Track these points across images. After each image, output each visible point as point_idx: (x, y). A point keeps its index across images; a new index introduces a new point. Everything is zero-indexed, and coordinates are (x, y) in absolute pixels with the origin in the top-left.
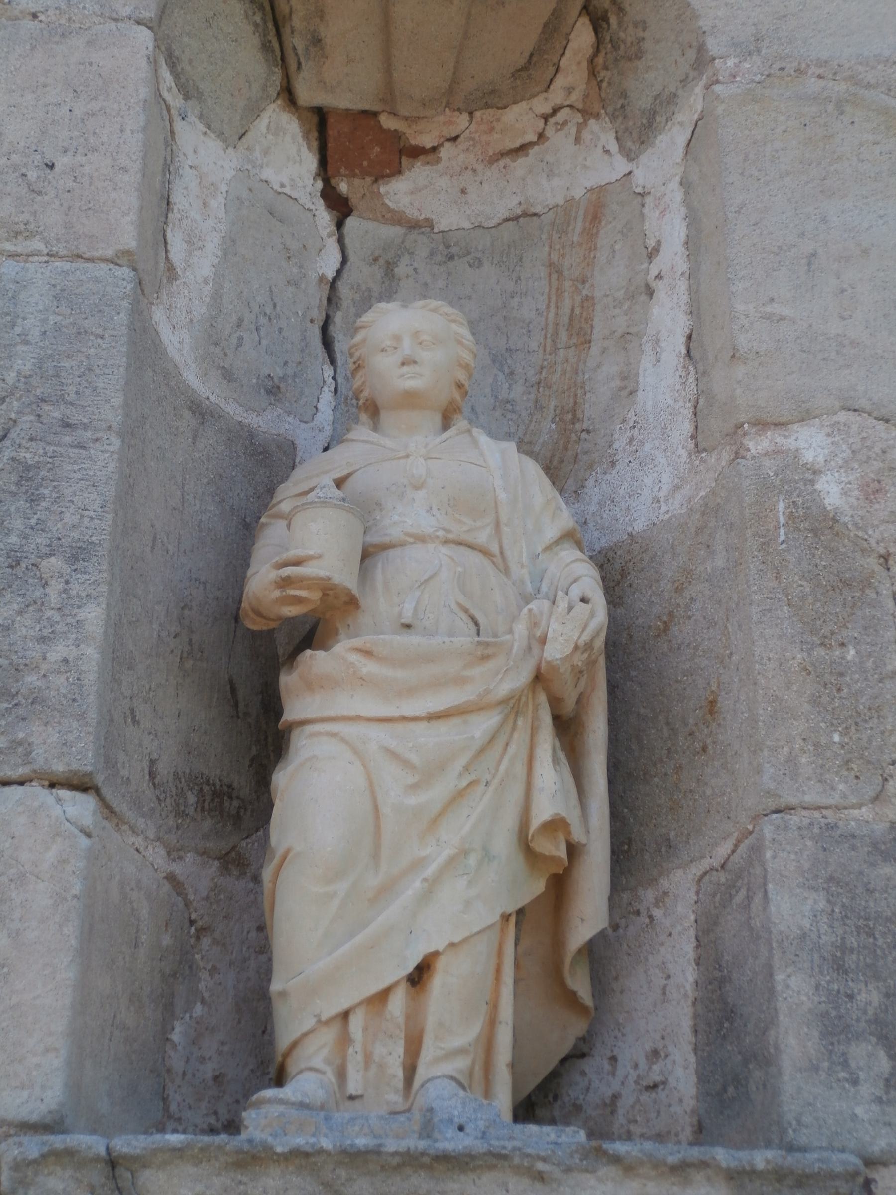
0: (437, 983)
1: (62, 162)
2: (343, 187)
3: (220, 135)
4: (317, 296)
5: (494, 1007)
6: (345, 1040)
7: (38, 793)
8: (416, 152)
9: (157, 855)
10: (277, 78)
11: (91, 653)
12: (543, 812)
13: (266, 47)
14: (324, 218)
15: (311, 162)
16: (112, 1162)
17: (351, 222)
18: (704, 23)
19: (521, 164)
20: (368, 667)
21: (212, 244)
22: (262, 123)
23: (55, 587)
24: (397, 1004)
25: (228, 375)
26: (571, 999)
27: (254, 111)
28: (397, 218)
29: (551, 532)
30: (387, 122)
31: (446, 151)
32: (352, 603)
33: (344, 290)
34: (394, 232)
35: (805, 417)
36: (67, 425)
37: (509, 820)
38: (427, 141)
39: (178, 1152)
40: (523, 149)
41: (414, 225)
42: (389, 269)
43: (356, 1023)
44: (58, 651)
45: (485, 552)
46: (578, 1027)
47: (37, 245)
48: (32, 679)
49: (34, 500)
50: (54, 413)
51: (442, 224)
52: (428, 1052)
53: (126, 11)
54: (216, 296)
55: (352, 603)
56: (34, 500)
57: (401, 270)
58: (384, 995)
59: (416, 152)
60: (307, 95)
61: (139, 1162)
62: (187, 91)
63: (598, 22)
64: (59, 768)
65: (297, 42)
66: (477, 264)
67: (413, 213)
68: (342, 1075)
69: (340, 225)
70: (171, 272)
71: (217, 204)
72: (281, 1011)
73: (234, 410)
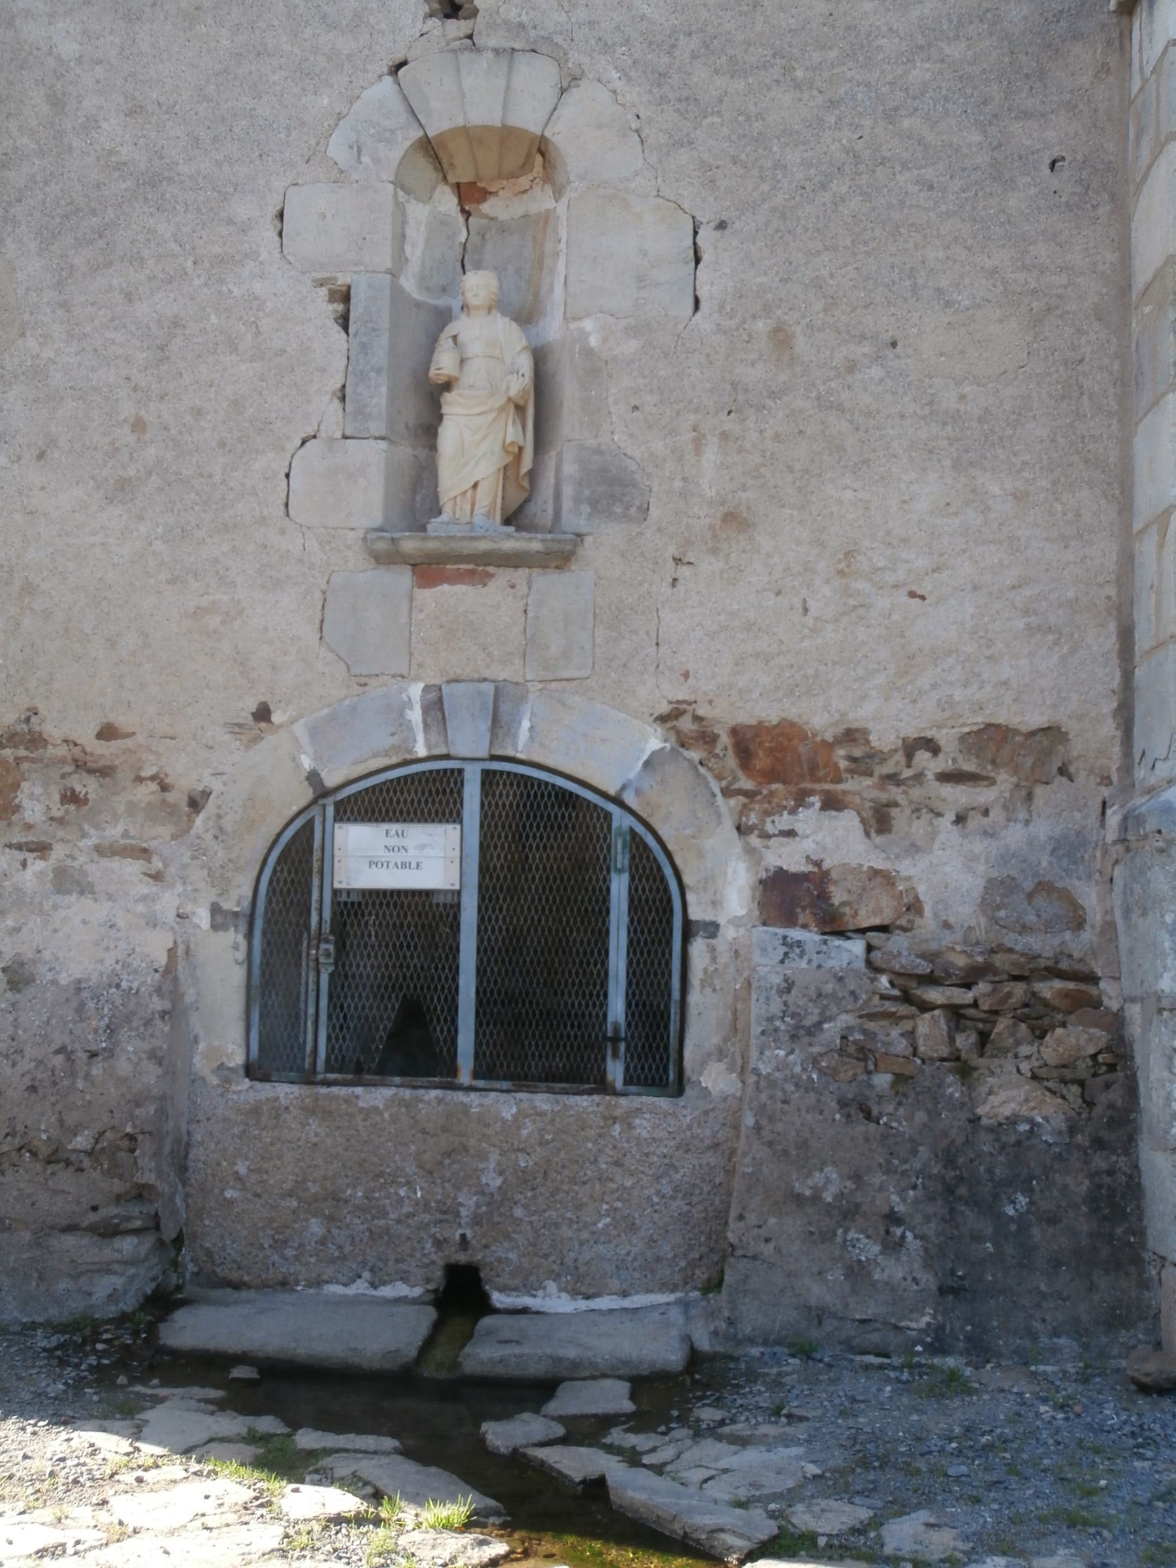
0: (479, 488)
1: (368, 237)
2: (467, 208)
3: (423, 202)
4: (458, 250)
5: (496, 492)
6: (455, 504)
7: (372, 442)
8: (491, 193)
9: (409, 451)
10: (441, 175)
11: (384, 401)
12: (508, 441)
13: (435, 168)
14: (461, 219)
15: (455, 200)
16: (393, 539)
17: (471, 219)
18: (569, 168)
19: (525, 196)
20: (460, 400)
21: (421, 245)
22: (437, 192)
23: (373, 381)
24: (469, 494)
25: (428, 289)
26: (523, 487)
27: (434, 189)
28: (486, 217)
29: (519, 348)
30: (479, 185)
31: (501, 192)
32: (457, 379)
33: (469, 246)
34: (484, 221)
35: (588, 315)
36: (374, 329)
37: (500, 442)
38: (493, 190)
39: (409, 537)
40: (526, 191)
41: (492, 219)
42: (483, 236)
43: (458, 499)
44: (374, 401)
45: (497, 358)
46: (526, 495)
47: (362, 268)
48: (368, 409)
49: (366, 354)
50: (370, 325)
51: (501, 218)
52: (477, 507)
53: (385, 178)
54: (423, 262)
55: (457, 379)
56: (366, 354)
57: (488, 237)
58: (465, 492)
59: (491, 193)
60: (452, 179)
61: (399, 539)
62: (408, 192)
63: (543, 154)
64: (377, 434)
65: (445, 166)
66: (511, 234)
67: (491, 215)
68: (454, 513)
69: (467, 220)
70: (407, 260)
71: (422, 229)
72: (441, 496)
73: (432, 301)
